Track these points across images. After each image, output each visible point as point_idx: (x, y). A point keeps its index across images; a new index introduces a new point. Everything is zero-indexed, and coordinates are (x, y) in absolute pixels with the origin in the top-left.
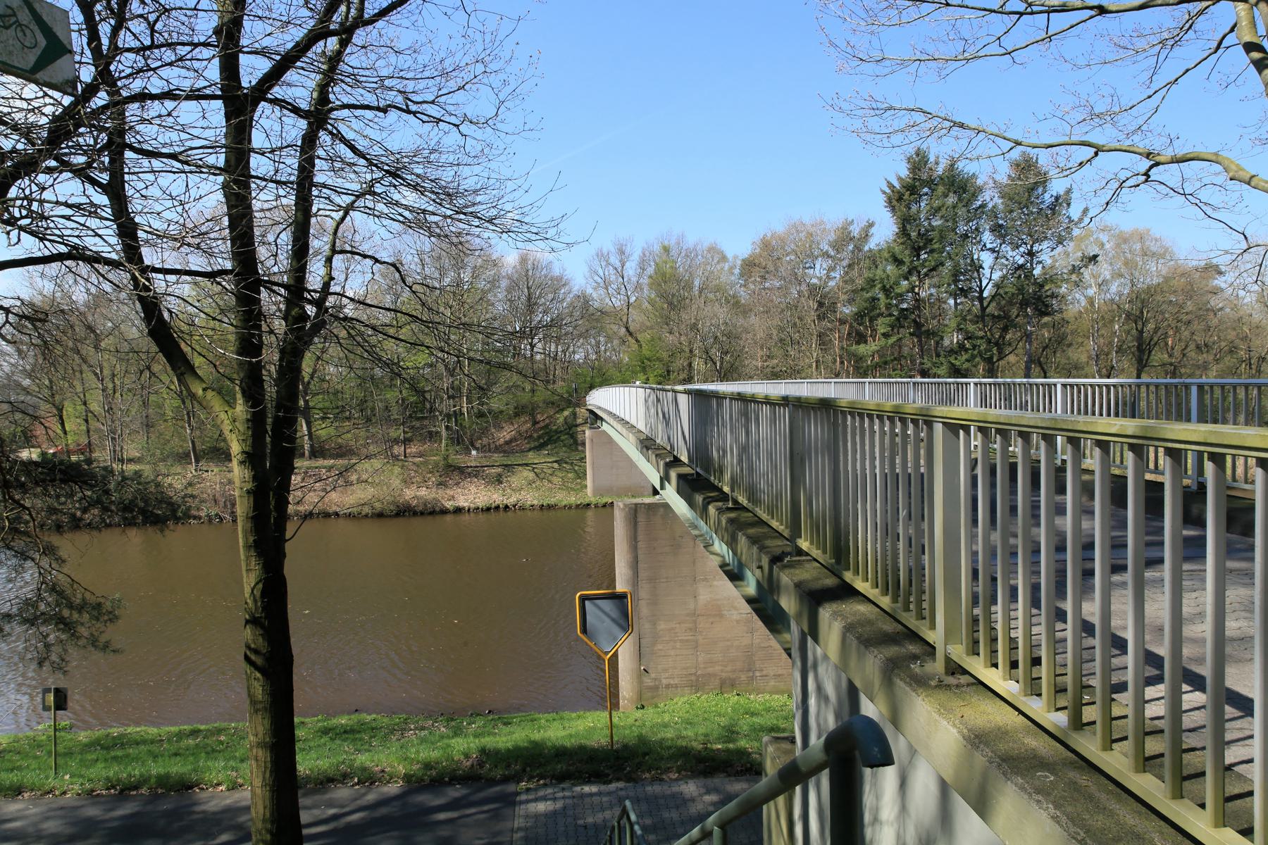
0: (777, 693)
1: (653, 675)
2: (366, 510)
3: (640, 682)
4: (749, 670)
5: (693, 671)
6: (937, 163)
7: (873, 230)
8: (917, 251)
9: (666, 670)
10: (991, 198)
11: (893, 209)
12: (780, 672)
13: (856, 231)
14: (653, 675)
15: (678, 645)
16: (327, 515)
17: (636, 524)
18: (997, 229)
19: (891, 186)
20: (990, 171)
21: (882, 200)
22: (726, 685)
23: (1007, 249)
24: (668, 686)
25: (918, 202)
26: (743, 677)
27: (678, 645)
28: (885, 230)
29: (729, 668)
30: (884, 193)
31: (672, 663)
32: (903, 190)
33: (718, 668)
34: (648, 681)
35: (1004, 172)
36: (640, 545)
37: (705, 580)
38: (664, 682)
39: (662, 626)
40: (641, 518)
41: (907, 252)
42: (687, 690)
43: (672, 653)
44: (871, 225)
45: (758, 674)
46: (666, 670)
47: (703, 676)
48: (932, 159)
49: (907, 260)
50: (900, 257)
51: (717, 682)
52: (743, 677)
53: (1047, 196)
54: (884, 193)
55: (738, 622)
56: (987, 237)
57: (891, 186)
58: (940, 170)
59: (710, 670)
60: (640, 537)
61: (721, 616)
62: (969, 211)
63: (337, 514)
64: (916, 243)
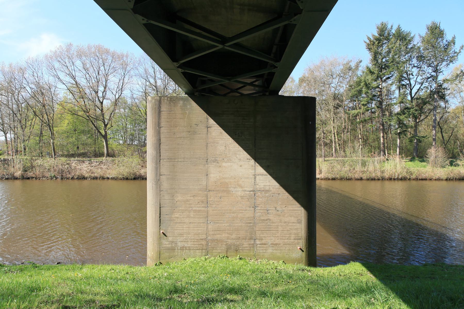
0: (274, 259)
1: (170, 239)
2: (121, 176)
3: (160, 244)
4: (251, 239)
5: (204, 236)
6: (391, 28)
7: (361, 64)
8: (381, 69)
9: (181, 235)
10: (417, 42)
11: (370, 49)
12: (277, 241)
13: (353, 65)
14: (170, 239)
15: (192, 214)
16: (103, 178)
17: (160, 112)
18: (421, 58)
19: (369, 38)
20: (418, 32)
21: (364, 46)
22: (232, 250)
23: (425, 67)
24: (182, 248)
25: (382, 46)
26: (246, 244)
27: (192, 214)
28: (366, 59)
29: (234, 236)
30: (365, 42)
31: (187, 228)
32: (375, 41)
33: (224, 235)
34: (166, 243)
35: (424, 32)
36: (162, 130)
37: (215, 161)
38: (180, 244)
39: (179, 198)
40: (164, 108)
41: (377, 69)
42: (198, 253)
43: (187, 220)
44: (361, 62)
45: (258, 242)
46: (181, 235)
47: (213, 241)
48: (389, 27)
49: (376, 72)
50: (372, 70)
51: (224, 247)
52: (246, 244)
53: (444, 41)
54: (365, 42)
55: (242, 197)
56: (415, 61)
57: (369, 38)
58: (393, 31)
59: (218, 237)
60: (163, 124)
61: (228, 192)
62: (407, 48)
63: (108, 178)
64: (381, 68)
